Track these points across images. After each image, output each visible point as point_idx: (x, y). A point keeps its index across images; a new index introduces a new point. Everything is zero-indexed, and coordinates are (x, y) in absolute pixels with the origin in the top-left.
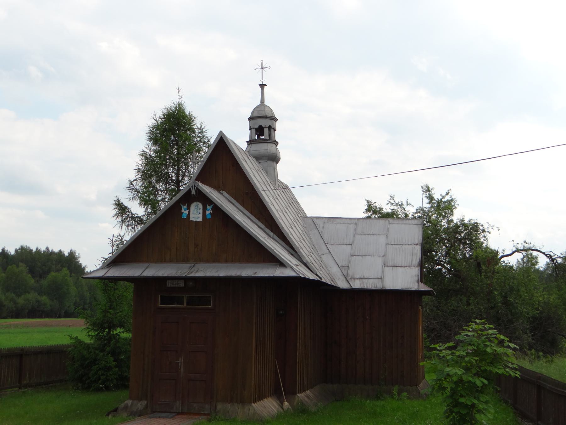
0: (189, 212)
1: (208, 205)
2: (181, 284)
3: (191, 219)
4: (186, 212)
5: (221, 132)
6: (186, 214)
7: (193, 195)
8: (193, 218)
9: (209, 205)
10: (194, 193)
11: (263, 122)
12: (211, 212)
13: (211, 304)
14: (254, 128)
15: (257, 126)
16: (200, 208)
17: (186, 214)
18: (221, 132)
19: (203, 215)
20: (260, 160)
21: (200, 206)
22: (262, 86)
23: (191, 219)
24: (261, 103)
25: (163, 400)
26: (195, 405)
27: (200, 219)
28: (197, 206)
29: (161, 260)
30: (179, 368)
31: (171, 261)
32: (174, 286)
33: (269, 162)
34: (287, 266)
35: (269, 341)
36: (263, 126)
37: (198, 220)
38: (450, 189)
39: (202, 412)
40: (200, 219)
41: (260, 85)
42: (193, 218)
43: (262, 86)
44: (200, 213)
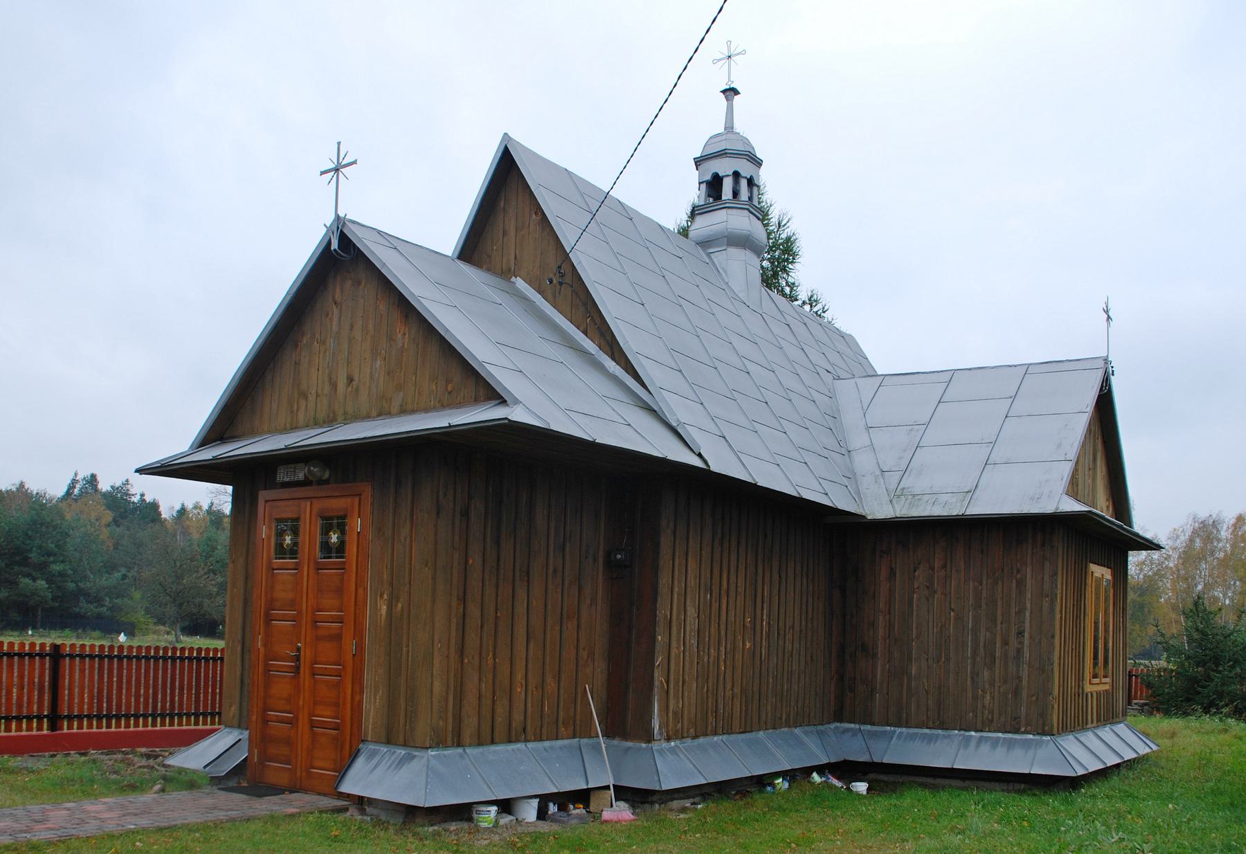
7: (335, 250)
10: (336, 247)
20: (710, 247)
22: (730, 92)
33: (733, 251)
41: (724, 92)
43: (730, 92)
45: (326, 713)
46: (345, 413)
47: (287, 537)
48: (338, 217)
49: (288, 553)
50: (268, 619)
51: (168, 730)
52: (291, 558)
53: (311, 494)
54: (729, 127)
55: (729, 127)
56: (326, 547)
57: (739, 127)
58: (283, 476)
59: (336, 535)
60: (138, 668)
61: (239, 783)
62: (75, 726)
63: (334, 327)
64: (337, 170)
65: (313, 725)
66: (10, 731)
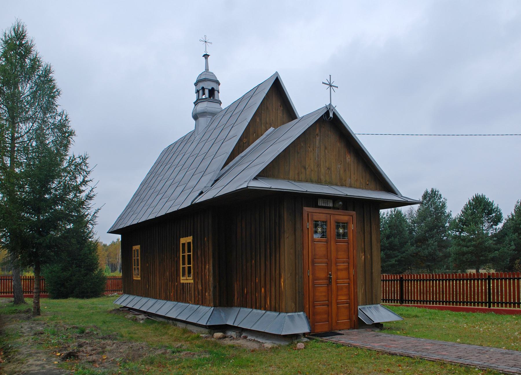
11: (209, 86)
15: (210, 88)
22: (206, 56)
34: (398, 194)
36: (215, 89)
43: (206, 56)
45: (343, 298)
46: (326, 181)
47: (319, 229)
49: (341, 236)
50: (313, 263)
51: (448, 307)
52: (343, 238)
53: (330, 212)
54: (207, 69)
55: (207, 69)
56: (338, 235)
57: (210, 70)
58: (321, 203)
59: (342, 230)
60: (28, 282)
61: (457, 322)
62: (496, 306)
63: (317, 144)
65: (338, 303)
66: (503, 307)
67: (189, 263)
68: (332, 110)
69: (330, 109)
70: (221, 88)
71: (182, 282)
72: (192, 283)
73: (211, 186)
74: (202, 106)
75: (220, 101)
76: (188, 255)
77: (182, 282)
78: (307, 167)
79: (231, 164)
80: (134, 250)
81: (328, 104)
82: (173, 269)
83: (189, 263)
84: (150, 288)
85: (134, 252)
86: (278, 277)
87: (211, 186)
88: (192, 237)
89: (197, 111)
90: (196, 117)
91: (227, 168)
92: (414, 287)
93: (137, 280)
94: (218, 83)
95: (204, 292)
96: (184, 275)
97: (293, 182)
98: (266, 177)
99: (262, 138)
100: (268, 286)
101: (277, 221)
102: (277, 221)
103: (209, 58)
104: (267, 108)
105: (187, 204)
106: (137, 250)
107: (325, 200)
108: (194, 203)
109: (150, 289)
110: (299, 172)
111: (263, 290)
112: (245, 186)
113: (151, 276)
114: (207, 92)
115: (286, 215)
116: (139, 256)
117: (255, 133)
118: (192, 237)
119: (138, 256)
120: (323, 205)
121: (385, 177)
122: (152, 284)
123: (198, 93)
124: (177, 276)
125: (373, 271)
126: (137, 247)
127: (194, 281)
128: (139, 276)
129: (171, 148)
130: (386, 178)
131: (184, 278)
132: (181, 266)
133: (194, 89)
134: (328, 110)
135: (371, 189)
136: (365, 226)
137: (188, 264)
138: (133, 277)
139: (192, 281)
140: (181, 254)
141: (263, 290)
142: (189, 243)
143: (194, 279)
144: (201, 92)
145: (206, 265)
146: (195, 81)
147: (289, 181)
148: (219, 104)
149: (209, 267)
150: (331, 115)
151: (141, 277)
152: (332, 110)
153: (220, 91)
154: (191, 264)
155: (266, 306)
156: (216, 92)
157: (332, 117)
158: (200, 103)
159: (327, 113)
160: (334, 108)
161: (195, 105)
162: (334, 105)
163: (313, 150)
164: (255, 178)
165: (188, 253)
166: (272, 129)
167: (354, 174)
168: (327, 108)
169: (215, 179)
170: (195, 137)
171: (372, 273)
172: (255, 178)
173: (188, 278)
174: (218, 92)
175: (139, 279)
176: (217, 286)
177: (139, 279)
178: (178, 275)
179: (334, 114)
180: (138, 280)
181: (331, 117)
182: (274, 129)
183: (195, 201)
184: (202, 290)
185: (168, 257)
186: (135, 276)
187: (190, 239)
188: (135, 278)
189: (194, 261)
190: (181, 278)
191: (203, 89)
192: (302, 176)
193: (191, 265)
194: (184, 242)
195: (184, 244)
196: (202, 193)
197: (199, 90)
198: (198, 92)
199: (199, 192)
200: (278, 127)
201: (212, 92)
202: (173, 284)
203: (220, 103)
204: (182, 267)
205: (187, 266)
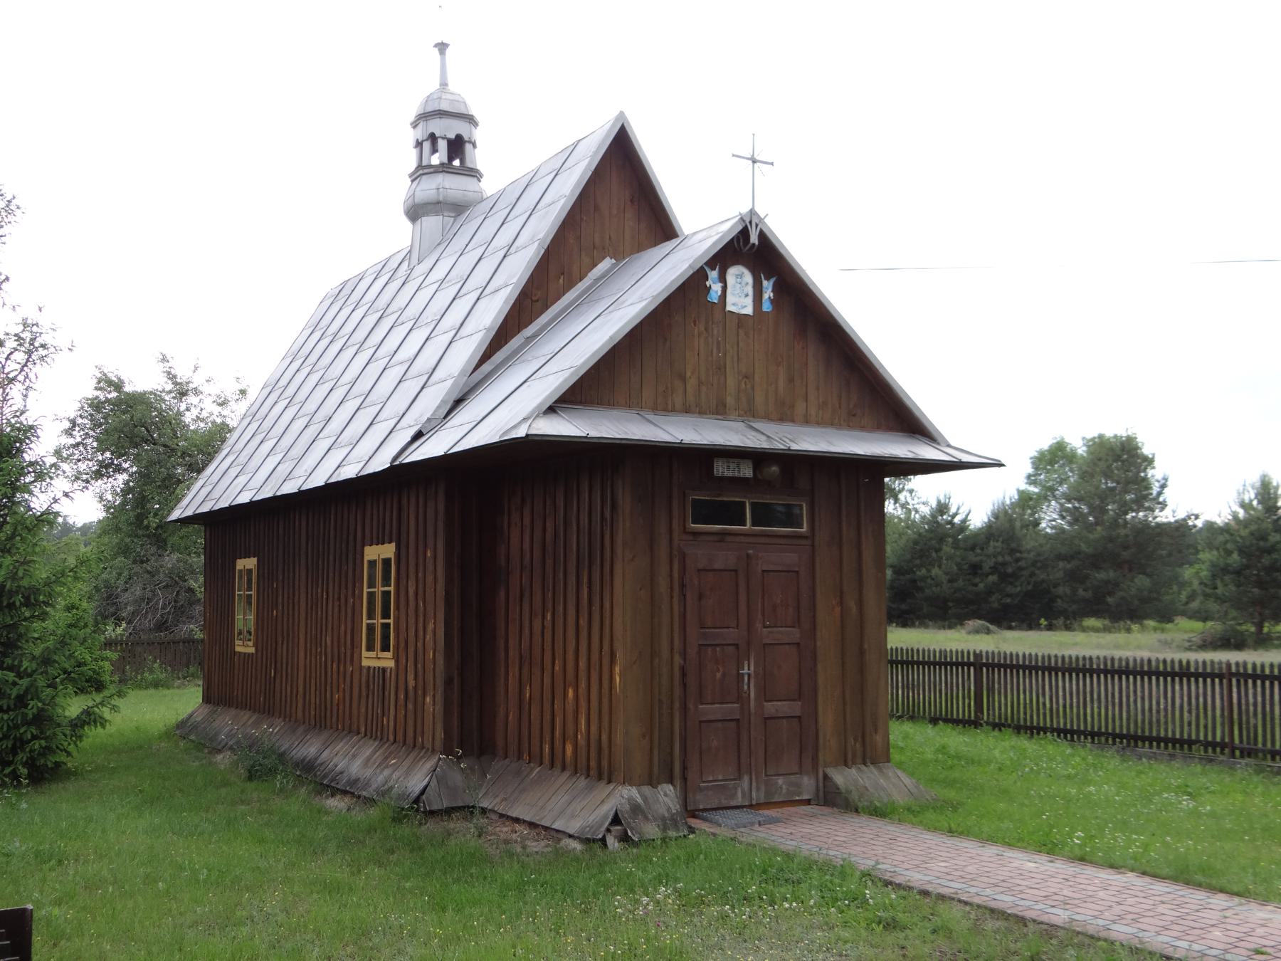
0: (724, 289)
1: (765, 279)
2: (747, 471)
3: (729, 308)
4: (716, 288)
5: (622, 114)
6: (717, 292)
8: (734, 304)
9: (768, 279)
11: (450, 129)
12: (772, 295)
13: (803, 525)
14: (443, 138)
15: (452, 136)
16: (747, 283)
17: (717, 292)
18: (622, 114)
19: (754, 301)
21: (748, 278)
22: (442, 47)
23: (729, 308)
24: (440, 85)
25: (711, 778)
26: (780, 781)
27: (749, 310)
28: (741, 276)
29: (664, 406)
30: (746, 687)
31: (687, 410)
32: (730, 474)
34: (939, 440)
35: (288, 627)
36: (466, 138)
37: (744, 311)
38: (96, 367)
39: (797, 798)
40: (749, 310)
42: (734, 304)
43: (442, 47)
44: (747, 295)
48: (752, 212)
54: (444, 84)
55: (444, 84)
64: (754, 162)
67: (386, 615)
68: (757, 225)
69: (750, 222)
70: (479, 135)
71: (365, 663)
72: (391, 669)
73: (445, 418)
74: (430, 187)
75: (476, 171)
76: (383, 625)
77: (365, 663)
78: (688, 374)
79: (499, 357)
80: (240, 571)
81: (745, 209)
82: (343, 627)
83: (386, 615)
84: (278, 676)
85: (240, 577)
86: (606, 661)
87: (445, 418)
88: (393, 545)
89: (417, 201)
90: (415, 212)
91: (486, 367)
92: (941, 697)
93: (245, 654)
94: (470, 120)
95: (420, 692)
96: (370, 648)
97: (651, 417)
98: (581, 403)
99: (581, 286)
100: (583, 685)
101: (608, 514)
102: (608, 514)
103: (448, 51)
104: (596, 208)
105: (381, 463)
106: (250, 571)
107: (732, 460)
108: (397, 463)
109: (278, 681)
110: (667, 388)
111: (571, 693)
112: (521, 433)
113: (282, 644)
114: (442, 145)
115: (626, 501)
116: (254, 586)
117: (563, 274)
118: (393, 545)
119: (249, 589)
120: (725, 474)
121: (902, 395)
122: (284, 666)
123: (418, 149)
124: (353, 648)
125: (866, 646)
126: (247, 563)
127: (397, 662)
128: (251, 644)
129: (347, 291)
130: (905, 399)
131: (372, 654)
132: (365, 621)
133: (411, 136)
134: (746, 226)
135: (863, 428)
136: (844, 528)
137: (383, 617)
138: (233, 646)
139: (391, 664)
140: (365, 590)
141: (571, 693)
142: (387, 562)
143: (397, 658)
144: (427, 146)
145: (428, 623)
146: (412, 118)
147: (641, 413)
148: (476, 179)
149: (435, 631)
150: (754, 239)
151: (256, 645)
152: (757, 225)
153: (478, 144)
154: (390, 618)
155: (577, 737)
156: (468, 147)
157: (757, 243)
158: (424, 177)
159: (744, 233)
160: (761, 220)
161: (412, 181)
162: (761, 211)
163: (706, 329)
164: (552, 410)
165: (383, 586)
166: (606, 264)
167: (818, 388)
168: (744, 221)
169: (455, 396)
170: (412, 267)
171: (862, 652)
172: (552, 410)
173: (382, 655)
174: (474, 145)
175: (252, 650)
176: (456, 681)
177: (252, 650)
178: (355, 645)
179: (762, 236)
180: (249, 654)
181: (754, 244)
182: (613, 261)
183: (400, 460)
184: (415, 688)
185: (331, 594)
186: (241, 643)
187: (388, 551)
188: (238, 649)
189: (397, 608)
190: (365, 654)
191: (433, 138)
192: (678, 401)
193: (391, 621)
194: (374, 557)
195: (372, 564)
196: (419, 435)
197: (423, 141)
198: (419, 144)
199: (412, 432)
200: (624, 258)
201: (457, 146)
202: (342, 668)
203: (474, 173)
204: (368, 593)
205: (378, 621)
